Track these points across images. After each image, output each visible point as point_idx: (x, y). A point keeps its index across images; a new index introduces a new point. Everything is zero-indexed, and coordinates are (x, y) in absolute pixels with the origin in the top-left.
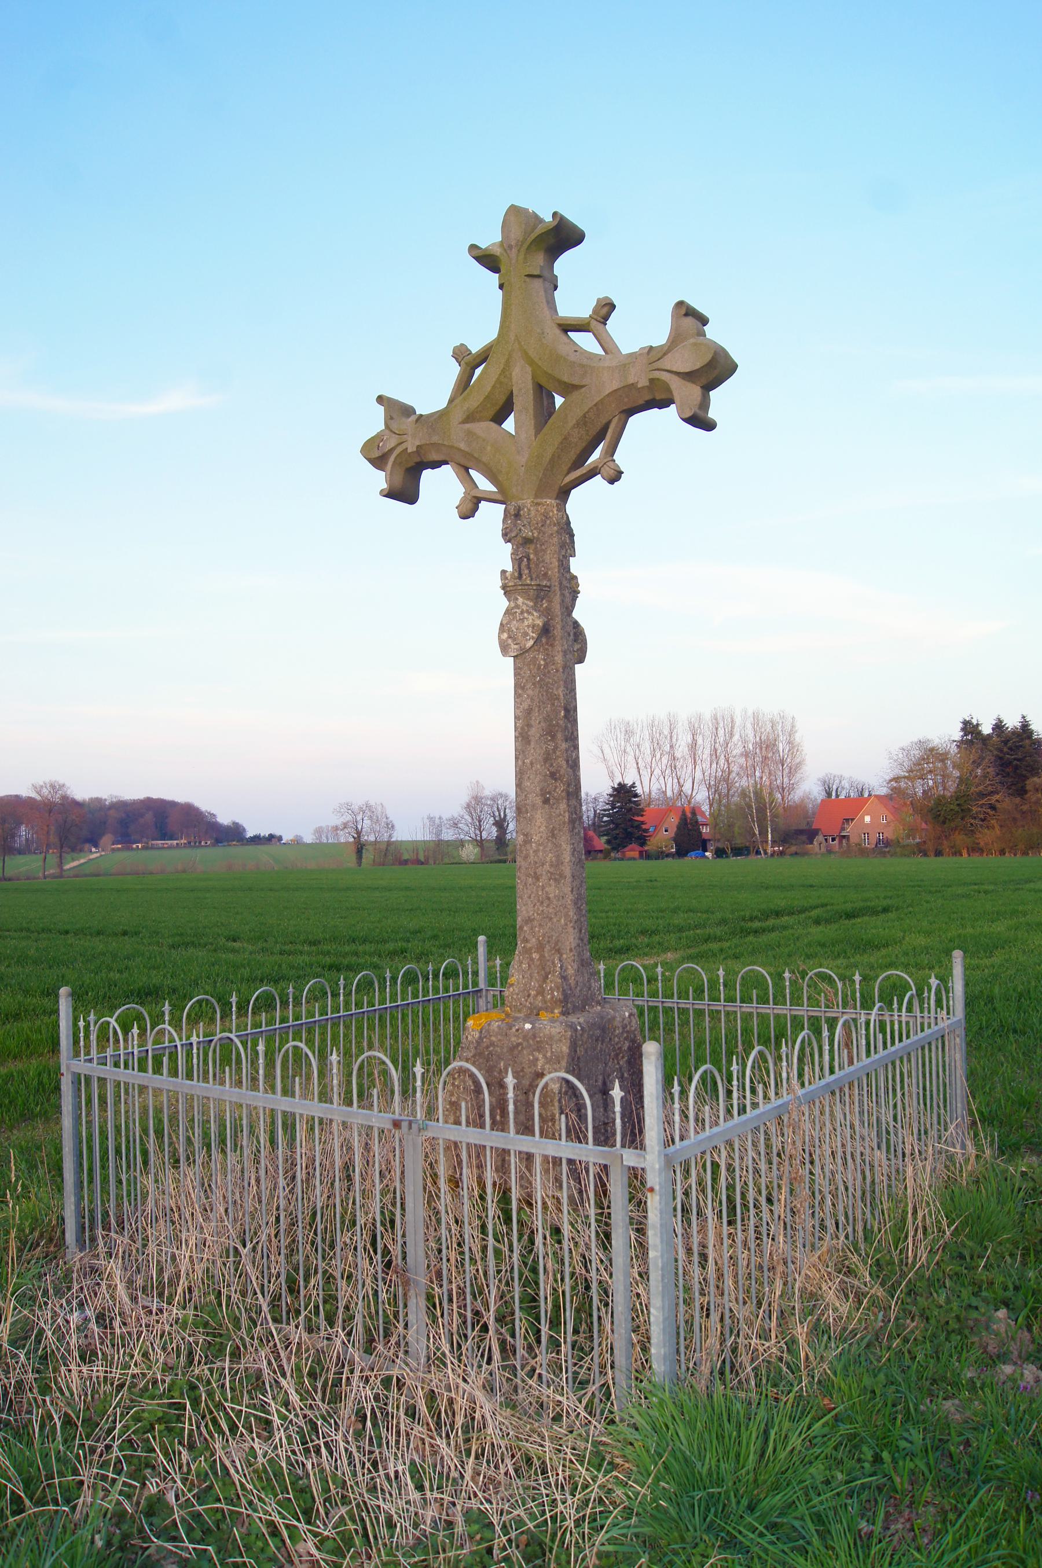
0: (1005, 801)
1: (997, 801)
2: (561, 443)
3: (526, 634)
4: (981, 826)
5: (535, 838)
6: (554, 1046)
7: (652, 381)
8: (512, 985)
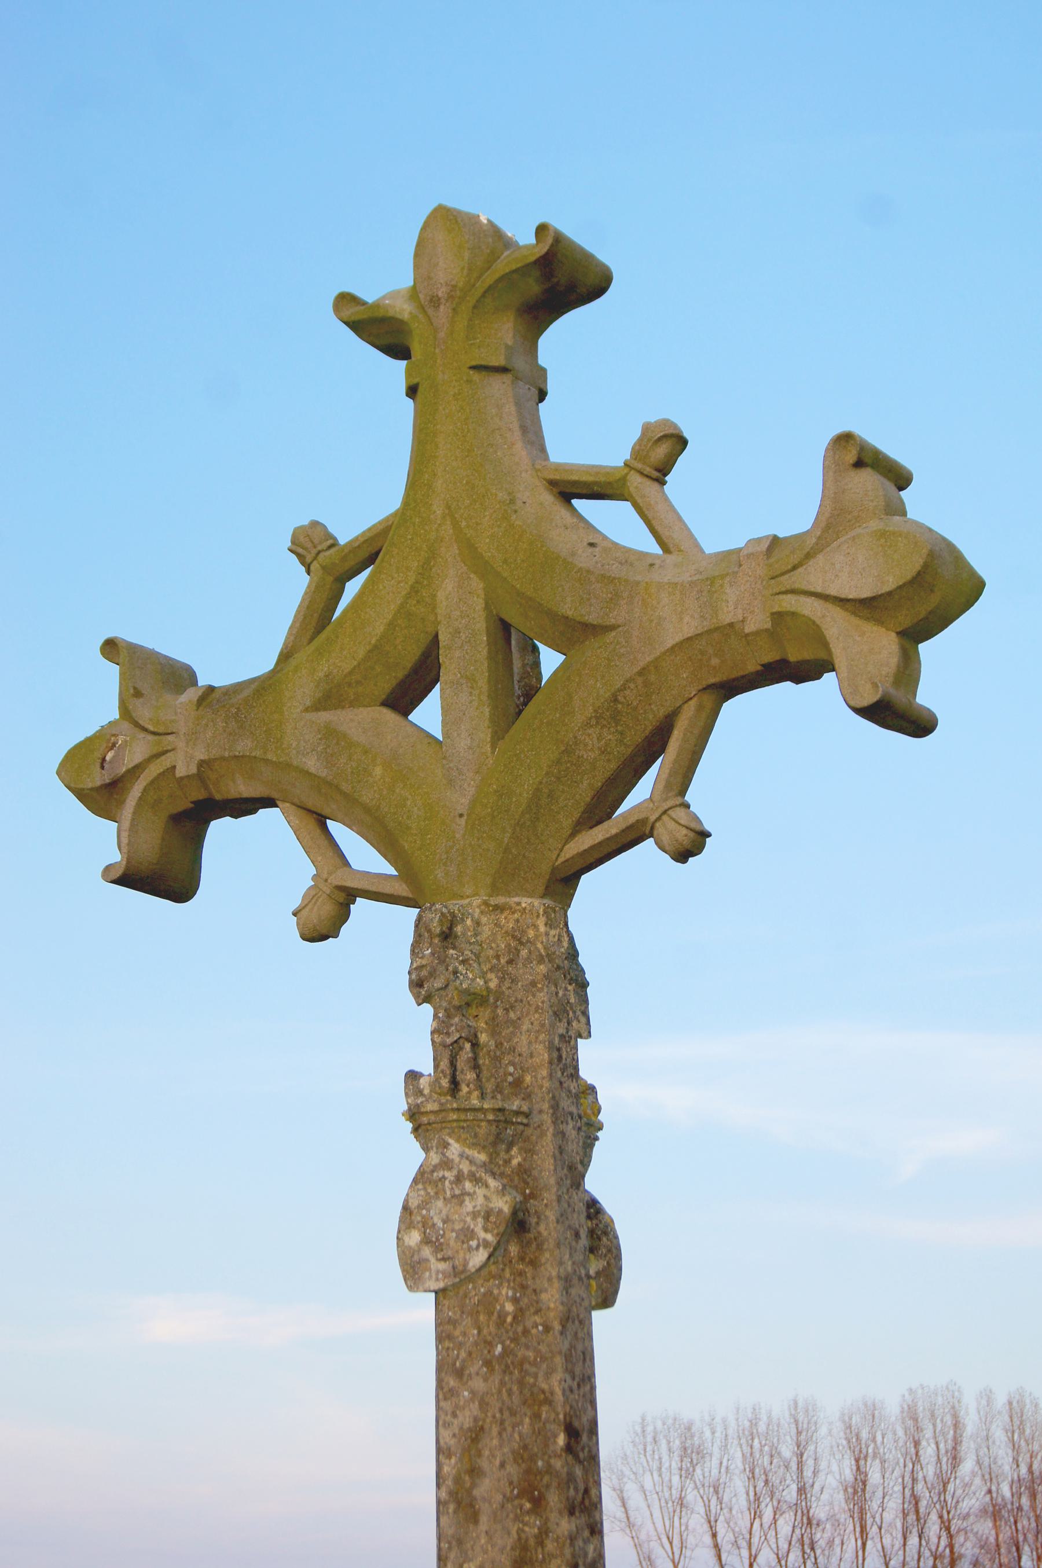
2: (558, 762)
3: (467, 1234)
7: (778, 617)
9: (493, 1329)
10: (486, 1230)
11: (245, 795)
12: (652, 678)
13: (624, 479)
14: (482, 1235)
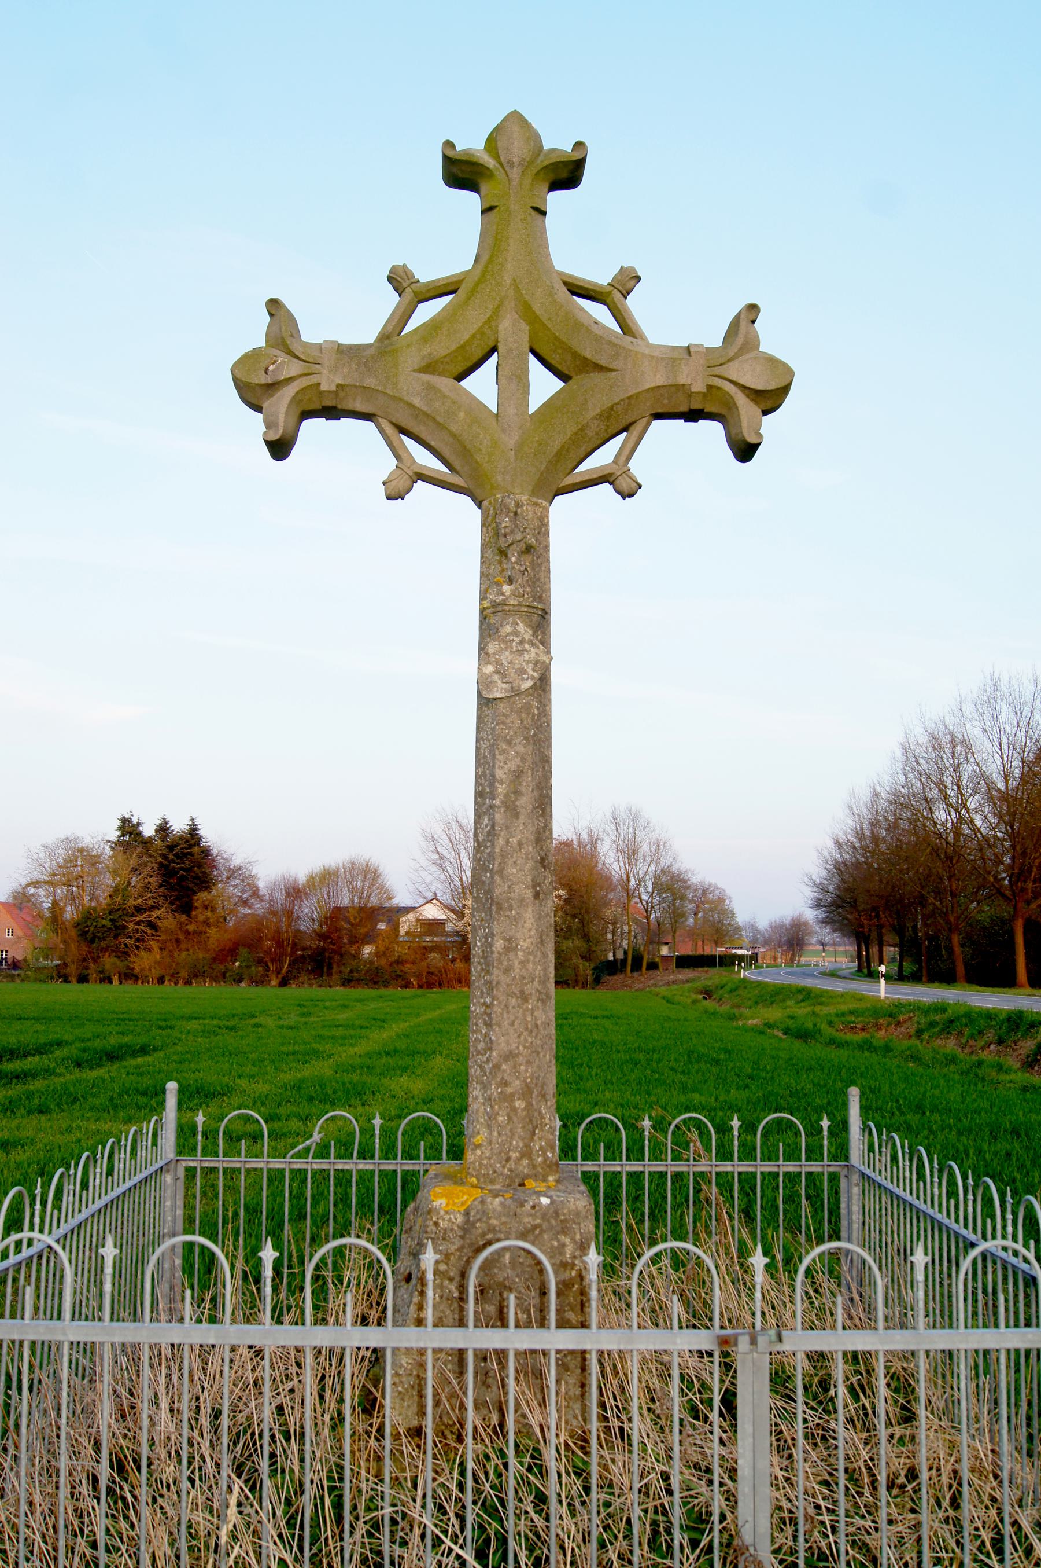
0: (167, 919)
1: (158, 918)
2: (576, 434)
3: (522, 671)
4: (137, 947)
5: (523, 944)
6: (582, 1225)
7: (710, 387)
8: (479, 1146)
9: (529, 721)
10: (534, 671)
11: (358, 409)
12: (633, 402)
13: (610, 293)
14: (531, 673)
